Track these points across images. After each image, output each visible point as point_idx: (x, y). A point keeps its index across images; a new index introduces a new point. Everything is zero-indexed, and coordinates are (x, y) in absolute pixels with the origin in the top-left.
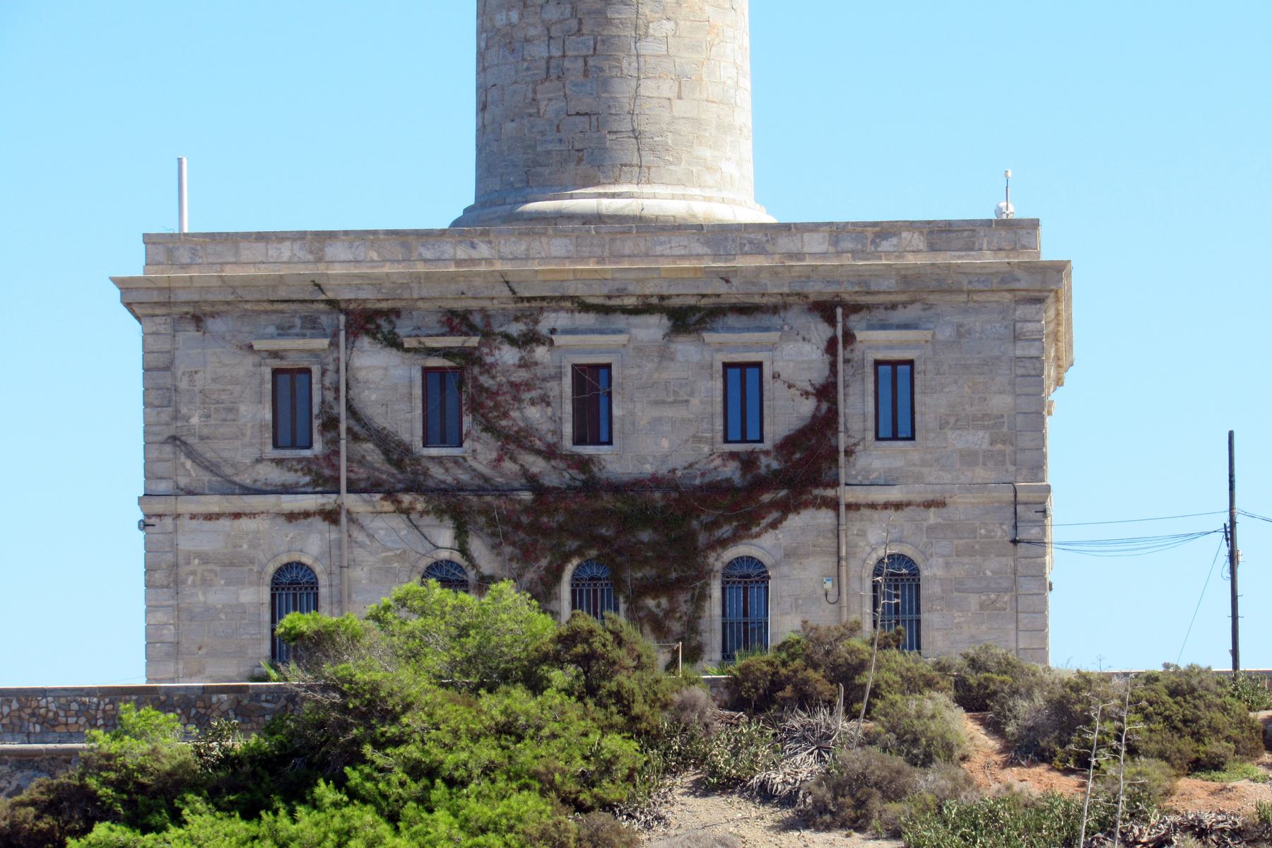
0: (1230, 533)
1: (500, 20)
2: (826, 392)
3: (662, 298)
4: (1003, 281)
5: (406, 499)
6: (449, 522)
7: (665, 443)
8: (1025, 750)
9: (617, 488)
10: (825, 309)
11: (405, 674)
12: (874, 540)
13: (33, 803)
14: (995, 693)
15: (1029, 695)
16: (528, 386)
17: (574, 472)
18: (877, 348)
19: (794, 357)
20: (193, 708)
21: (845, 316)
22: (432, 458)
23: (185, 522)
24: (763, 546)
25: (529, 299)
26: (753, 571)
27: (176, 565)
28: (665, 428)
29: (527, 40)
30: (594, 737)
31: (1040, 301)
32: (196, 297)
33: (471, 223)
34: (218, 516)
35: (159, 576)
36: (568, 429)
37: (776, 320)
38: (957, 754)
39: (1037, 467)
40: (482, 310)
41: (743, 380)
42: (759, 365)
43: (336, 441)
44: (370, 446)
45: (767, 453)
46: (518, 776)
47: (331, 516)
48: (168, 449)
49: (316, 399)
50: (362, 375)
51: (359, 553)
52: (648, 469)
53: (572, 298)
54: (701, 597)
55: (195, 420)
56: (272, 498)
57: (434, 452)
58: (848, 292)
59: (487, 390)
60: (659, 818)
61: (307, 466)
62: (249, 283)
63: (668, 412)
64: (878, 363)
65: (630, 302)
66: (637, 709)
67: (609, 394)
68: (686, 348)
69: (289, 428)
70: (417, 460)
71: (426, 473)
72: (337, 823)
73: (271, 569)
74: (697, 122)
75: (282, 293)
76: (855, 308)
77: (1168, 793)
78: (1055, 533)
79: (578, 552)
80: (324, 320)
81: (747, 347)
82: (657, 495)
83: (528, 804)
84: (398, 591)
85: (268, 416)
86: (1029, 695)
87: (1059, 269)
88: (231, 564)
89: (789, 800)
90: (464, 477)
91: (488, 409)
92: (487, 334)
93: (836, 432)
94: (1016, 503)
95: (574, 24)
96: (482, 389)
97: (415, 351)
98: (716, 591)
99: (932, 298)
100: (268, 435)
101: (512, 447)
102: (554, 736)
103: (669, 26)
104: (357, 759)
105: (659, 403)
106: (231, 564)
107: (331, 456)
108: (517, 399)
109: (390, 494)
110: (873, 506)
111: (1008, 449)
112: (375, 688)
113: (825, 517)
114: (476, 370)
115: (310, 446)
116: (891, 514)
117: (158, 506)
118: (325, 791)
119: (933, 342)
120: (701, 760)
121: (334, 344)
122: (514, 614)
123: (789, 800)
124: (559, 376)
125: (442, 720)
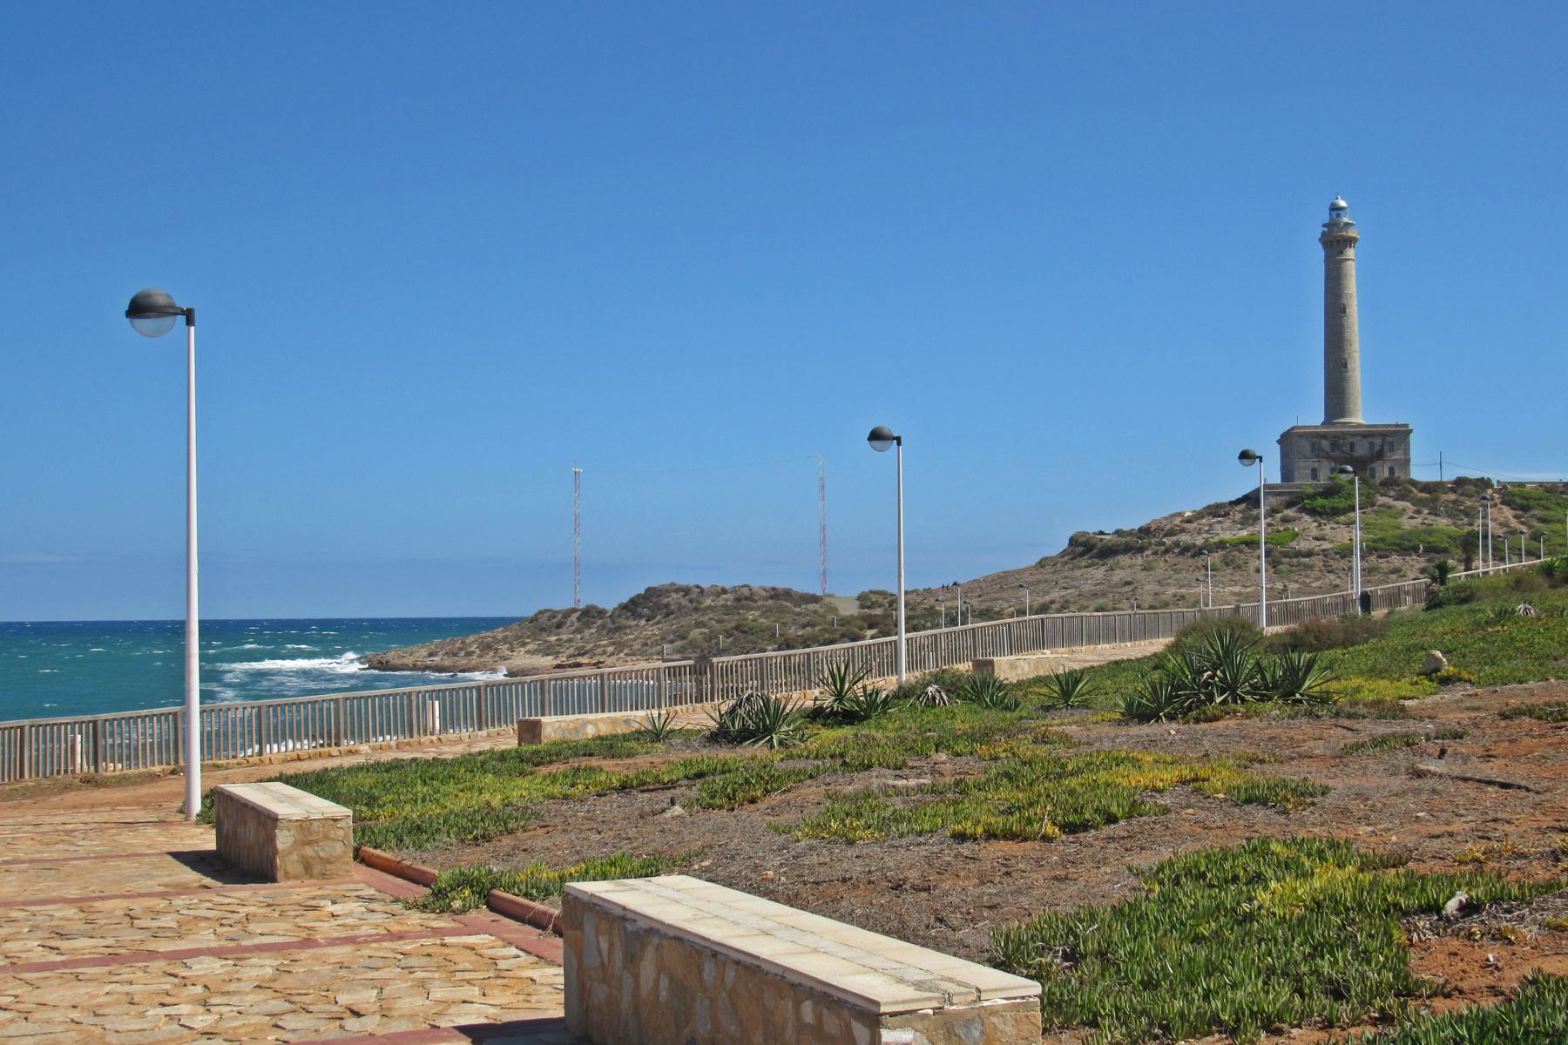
8: (1421, 491)
19: (1378, 441)
28: (1361, 450)
33: (1326, 423)
41: (1372, 444)
69: (1313, 451)
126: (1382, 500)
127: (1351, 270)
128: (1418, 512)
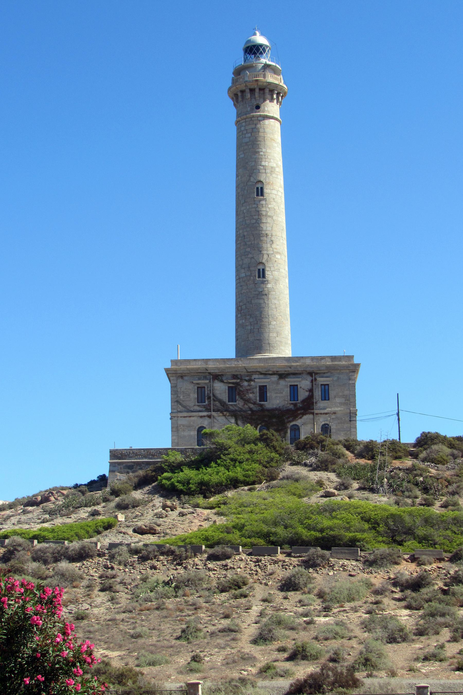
0: (398, 414)
1: (241, 322)
2: (311, 391)
3: (277, 371)
4: (347, 367)
5: (225, 413)
6: (234, 418)
7: (278, 401)
8: (360, 455)
9: (268, 410)
10: (310, 374)
11: (229, 441)
12: (321, 421)
13: (151, 470)
14: (351, 446)
15: (359, 445)
16: (250, 390)
17: (259, 407)
18: (321, 382)
19: (304, 384)
20: (182, 451)
21: (315, 375)
22: (230, 405)
23: (179, 418)
24: (298, 422)
25: (250, 372)
26: (296, 427)
27: (178, 427)
28: (278, 398)
29: (246, 326)
30: (269, 454)
31: (354, 372)
32: (181, 372)
34: (186, 417)
35: (174, 429)
36: (258, 398)
37: (300, 376)
38: (345, 457)
39: (355, 406)
40: (240, 374)
41: (294, 389)
42: (297, 385)
43: (210, 401)
44: (217, 402)
45: (299, 403)
46: (254, 461)
47: (209, 417)
48: (176, 403)
49: (206, 393)
50: (216, 388)
51: (215, 424)
52: (275, 406)
53: (259, 372)
54: (286, 433)
55: (181, 397)
56: (197, 413)
57: (230, 403)
58: (315, 370)
59: (241, 391)
60: (283, 470)
61: (204, 406)
62: (193, 369)
63: (279, 395)
64: (321, 385)
65: (270, 372)
66: (277, 449)
67: (266, 392)
68: (282, 382)
70: (227, 405)
71: (229, 408)
72: (216, 470)
73: (197, 427)
74: (281, 342)
75: (199, 371)
76: (316, 374)
77: (391, 463)
78: (358, 418)
79: (261, 424)
80: (208, 377)
81: (295, 382)
82: (277, 412)
83: (256, 466)
84: (226, 427)
85: (196, 396)
86: (359, 445)
87: (357, 366)
88: (189, 427)
89: (311, 466)
90: (237, 409)
91: (242, 395)
92: (241, 379)
93: (313, 399)
94: (350, 413)
95: (256, 322)
96: (240, 391)
97: (226, 383)
98: (289, 431)
99: (333, 371)
100: (196, 400)
101: (246, 402)
102: (260, 453)
103: (275, 322)
104: (220, 458)
105: (276, 393)
106: (189, 427)
107: (209, 404)
108: (248, 393)
109: (222, 412)
110: (321, 414)
111: (349, 402)
112: (223, 443)
113: (311, 416)
114: (239, 387)
115: (205, 402)
116: (324, 416)
117: (174, 415)
118: (213, 464)
119: (333, 380)
120: (291, 459)
121: (210, 382)
122: (251, 431)
123: (311, 466)
124: (256, 388)
125: (237, 451)
126: (289, 469)
127: (273, 134)
128: (343, 487)
